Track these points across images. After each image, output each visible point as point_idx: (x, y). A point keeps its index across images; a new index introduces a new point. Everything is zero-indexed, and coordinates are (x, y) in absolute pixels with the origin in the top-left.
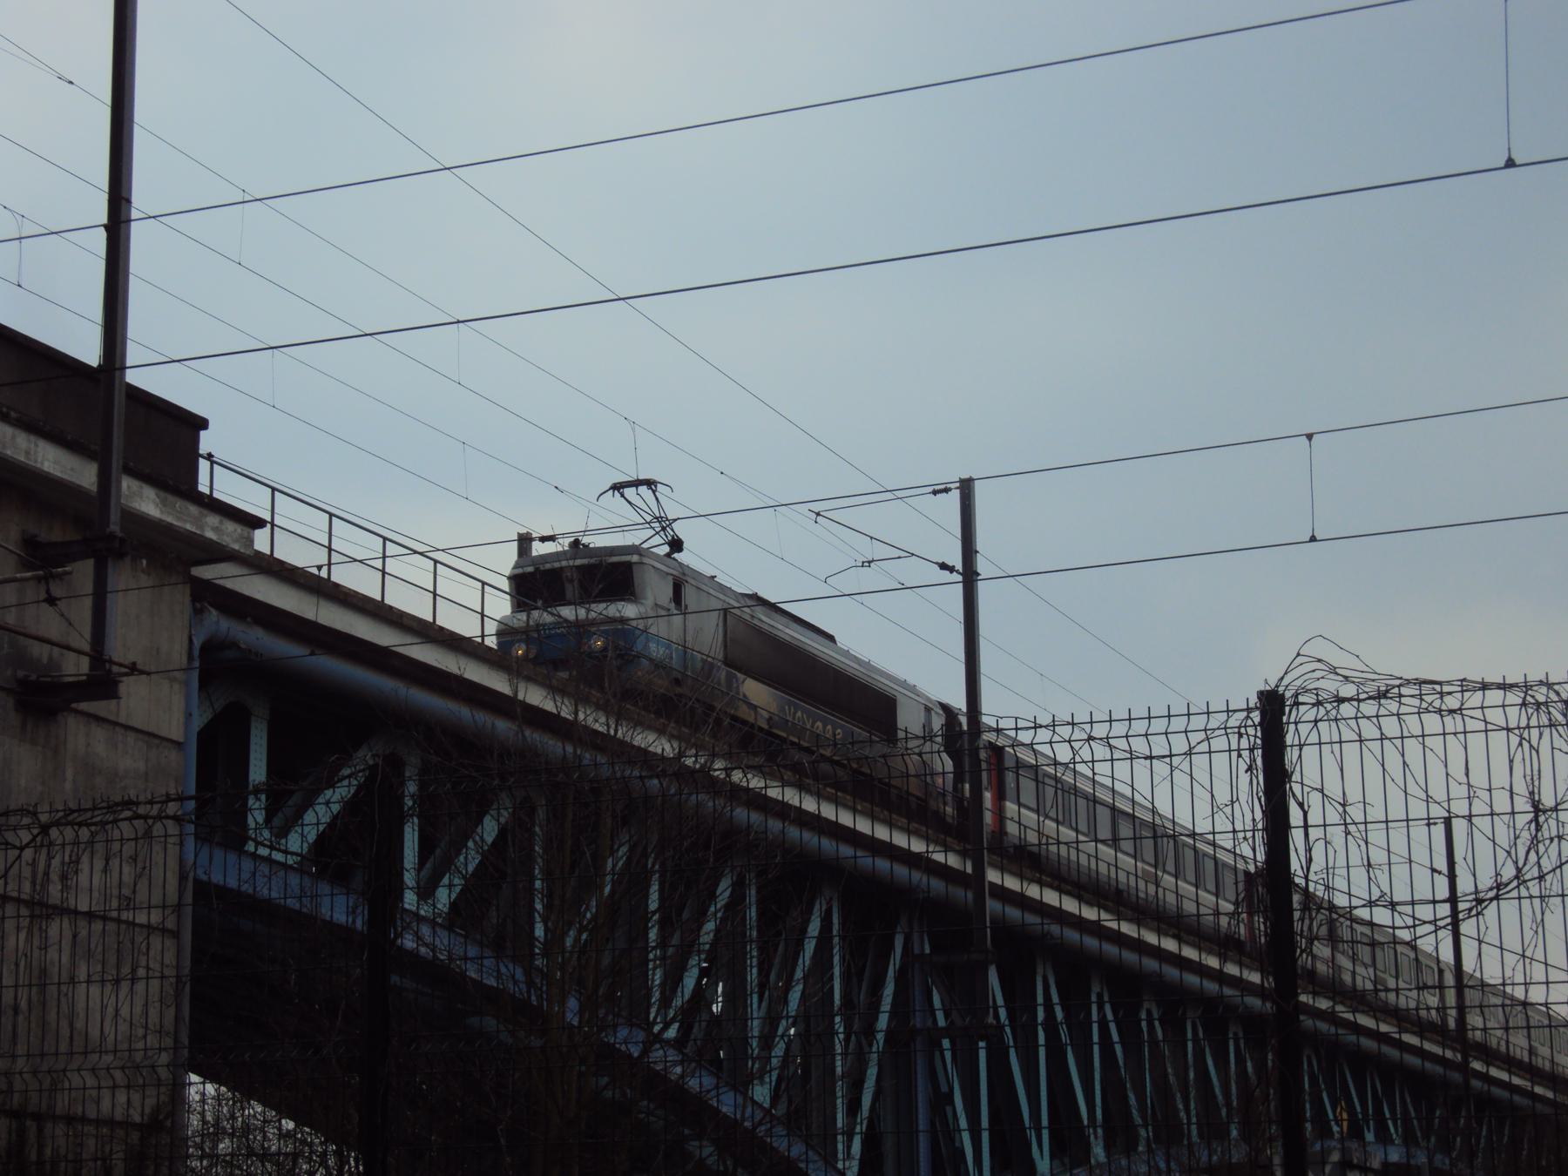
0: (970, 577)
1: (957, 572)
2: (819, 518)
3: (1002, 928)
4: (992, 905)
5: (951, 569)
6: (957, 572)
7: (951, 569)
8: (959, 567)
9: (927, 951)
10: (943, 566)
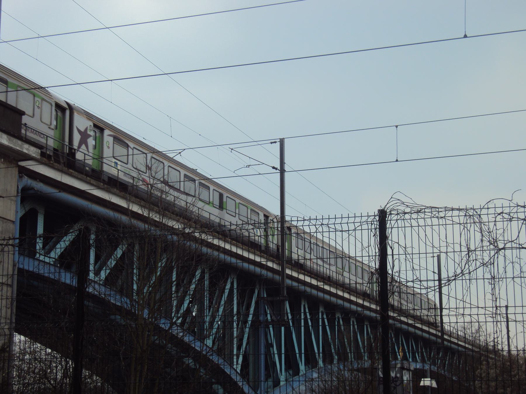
0: (282, 171)
1: (278, 170)
2: (232, 151)
3: (290, 289)
4: (288, 282)
5: (276, 169)
6: (278, 170)
7: (276, 169)
8: (279, 168)
9: (265, 296)
10: (274, 168)
